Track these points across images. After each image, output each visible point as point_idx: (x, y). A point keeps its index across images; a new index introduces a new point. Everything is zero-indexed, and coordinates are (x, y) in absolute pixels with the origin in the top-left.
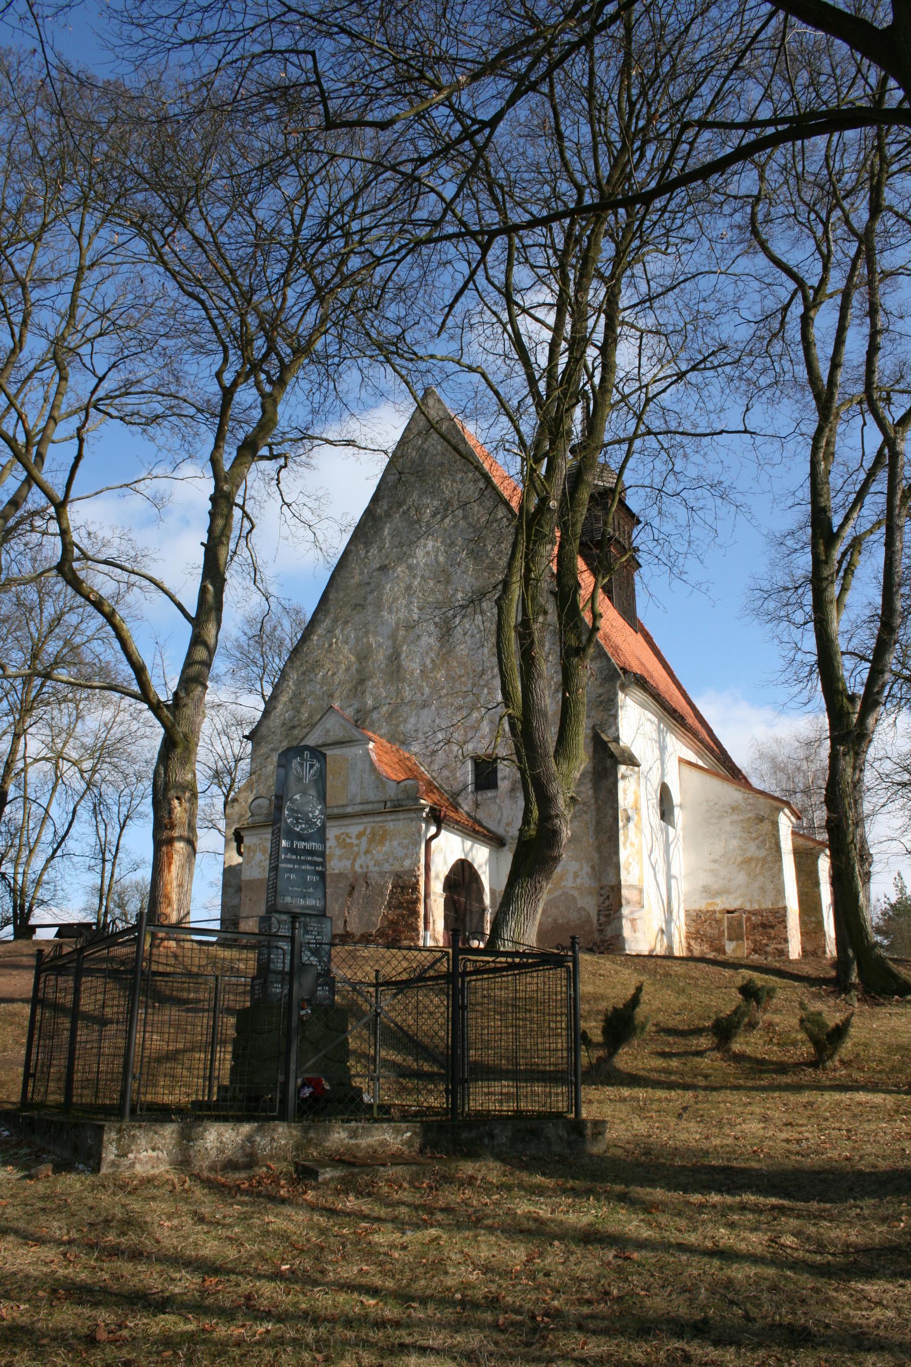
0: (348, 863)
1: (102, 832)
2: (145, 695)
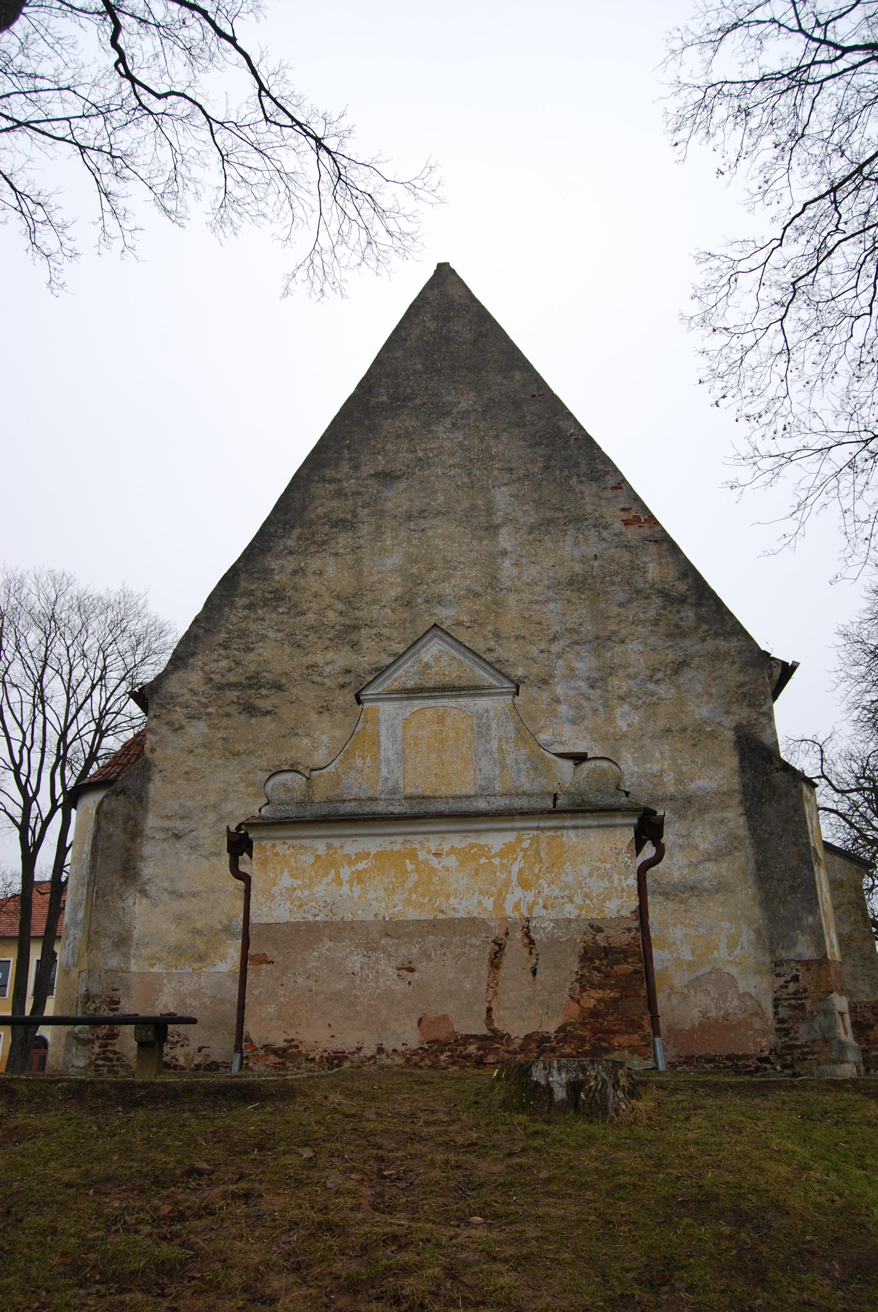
0: (489, 903)
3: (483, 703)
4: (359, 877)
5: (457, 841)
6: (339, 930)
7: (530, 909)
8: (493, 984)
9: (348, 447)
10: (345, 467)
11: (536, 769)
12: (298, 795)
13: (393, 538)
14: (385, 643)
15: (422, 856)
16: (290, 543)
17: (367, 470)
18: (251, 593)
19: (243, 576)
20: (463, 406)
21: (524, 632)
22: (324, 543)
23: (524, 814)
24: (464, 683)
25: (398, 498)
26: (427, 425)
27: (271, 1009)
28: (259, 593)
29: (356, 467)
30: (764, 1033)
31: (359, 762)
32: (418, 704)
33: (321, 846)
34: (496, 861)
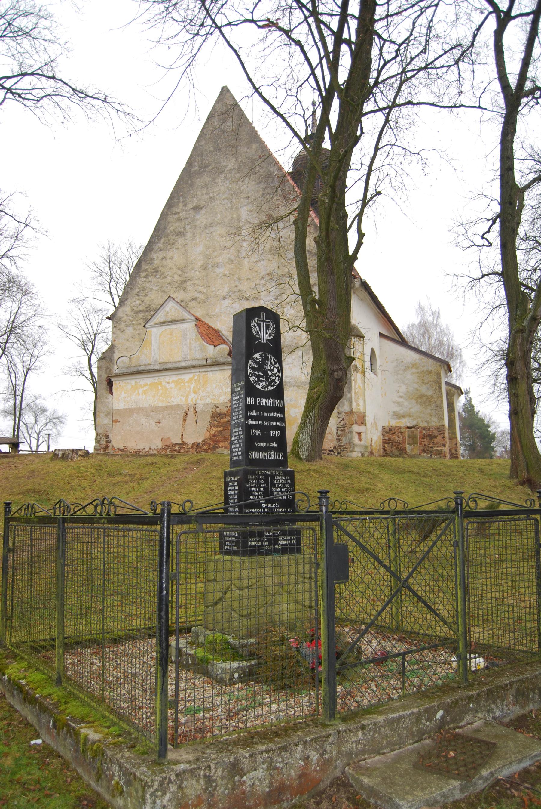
0: (183, 399)
1: (13, 379)
2: (304, 117)
3: (185, 325)
4: (145, 392)
5: (174, 378)
6: (138, 410)
7: (196, 401)
8: (184, 427)
9: (182, 195)
10: (181, 205)
11: (201, 350)
12: (127, 365)
13: (200, 238)
14: (196, 287)
15: (164, 384)
16: (160, 245)
17: (190, 206)
18: (146, 270)
19: (143, 263)
20: (230, 167)
21: (250, 277)
22: (173, 244)
23: (194, 367)
24: (179, 318)
25: (202, 218)
26: (214, 179)
27: (119, 437)
28: (149, 270)
29: (185, 205)
30: (332, 441)
31: (145, 351)
32: (164, 328)
33: (133, 382)
34: (186, 384)
